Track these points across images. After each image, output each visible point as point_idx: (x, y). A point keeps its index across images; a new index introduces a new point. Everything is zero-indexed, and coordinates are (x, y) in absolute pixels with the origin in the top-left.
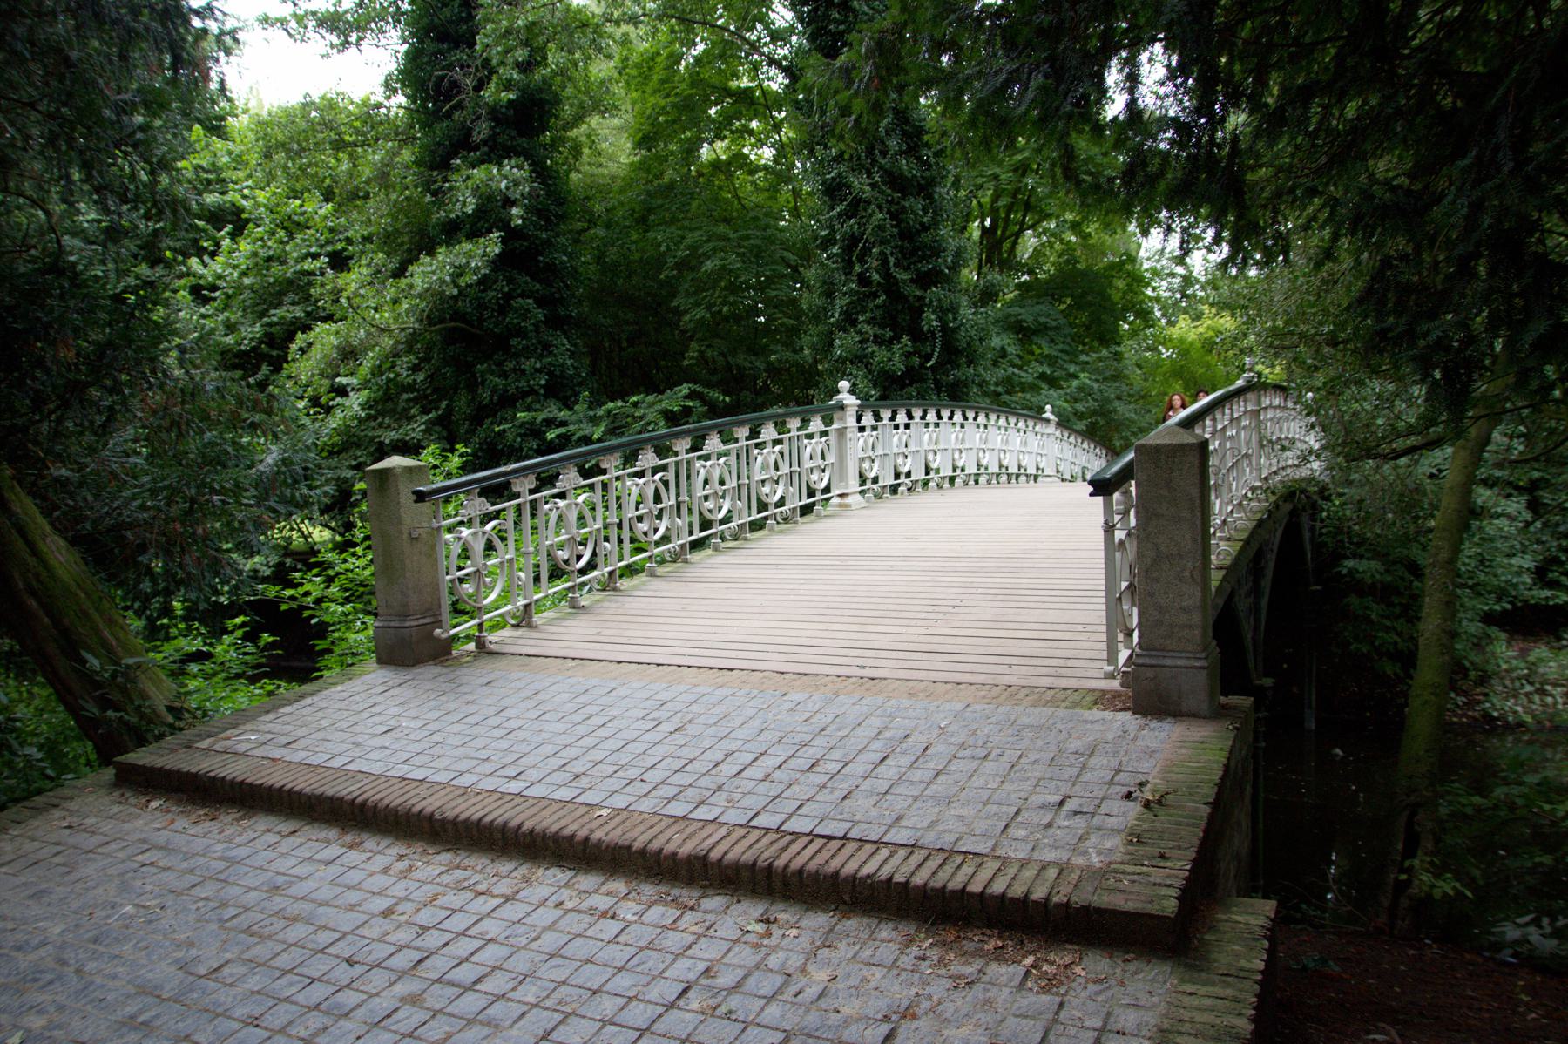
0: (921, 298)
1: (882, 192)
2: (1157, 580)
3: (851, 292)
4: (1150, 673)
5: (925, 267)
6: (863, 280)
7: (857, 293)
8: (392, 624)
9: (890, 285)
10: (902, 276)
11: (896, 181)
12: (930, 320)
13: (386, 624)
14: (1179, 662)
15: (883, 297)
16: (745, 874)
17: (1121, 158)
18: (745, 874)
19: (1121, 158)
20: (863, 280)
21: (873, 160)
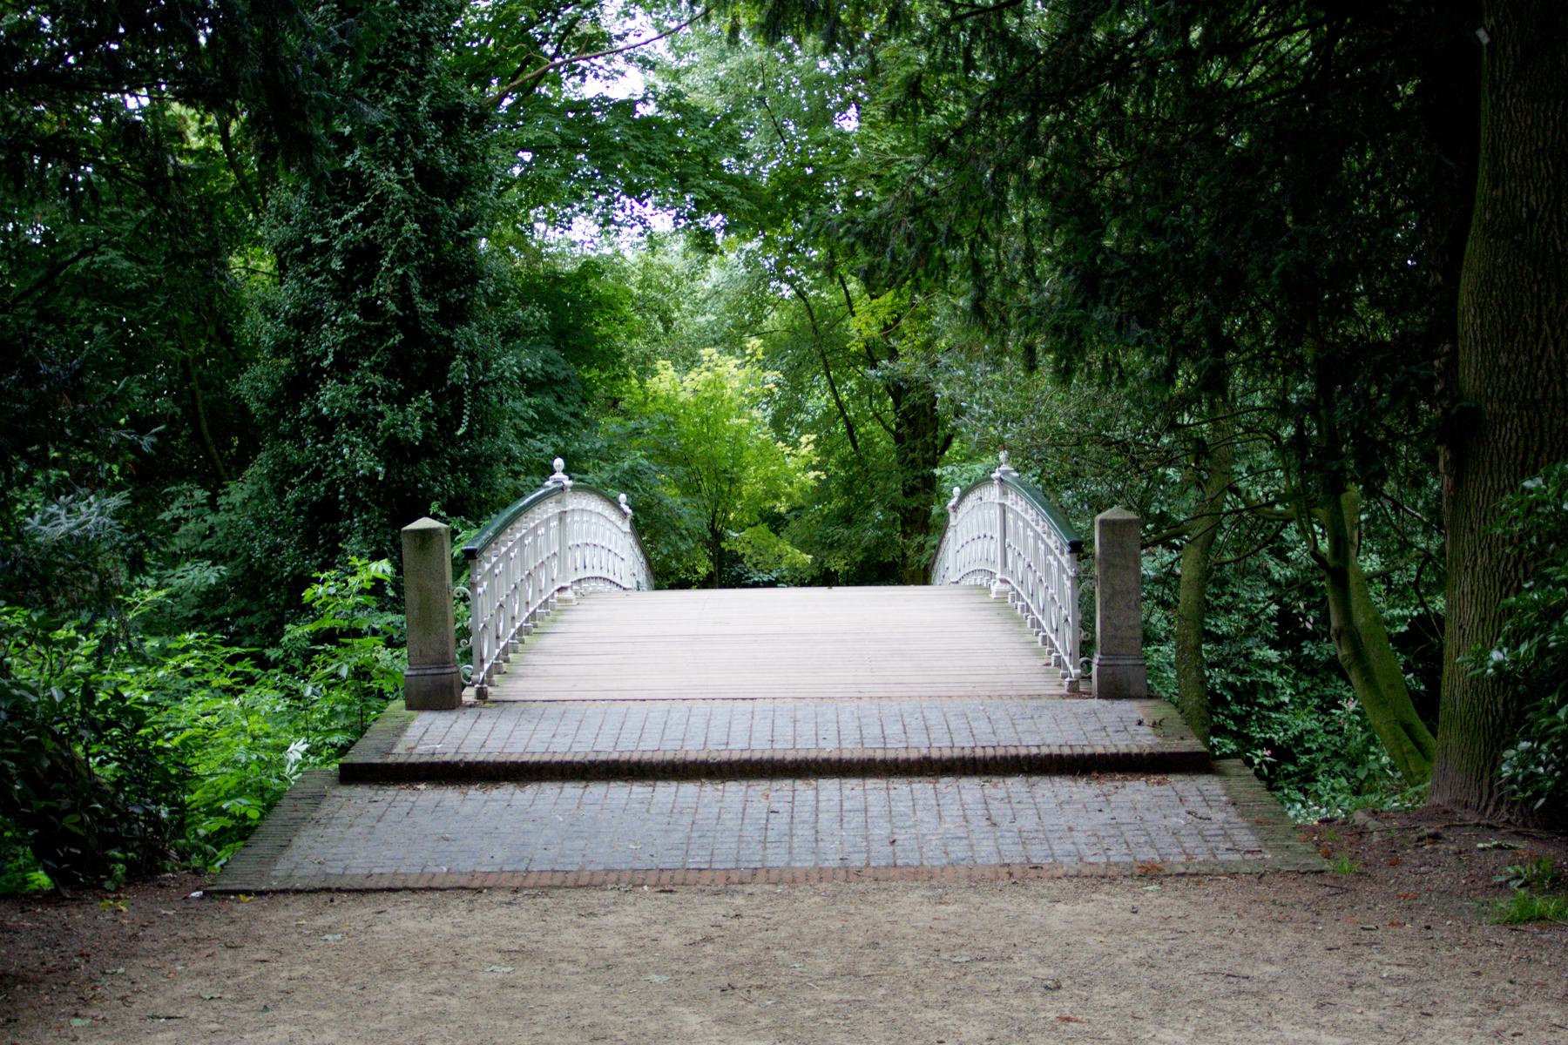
0: (449, 340)
1: (411, 191)
2: (1113, 608)
3: (348, 326)
4: (1109, 670)
5: (454, 296)
6: (369, 309)
7: (357, 326)
8: (429, 672)
9: (409, 322)
10: (425, 307)
11: (429, 177)
12: (459, 370)
13: (420, 672)
14: (1128, 662)
15: (399, 337)
16: (959, 764)
17: (543, 90)
18: (959, 764)
19: (543, 90)
20: (369, 309)
21: (403, 148)
